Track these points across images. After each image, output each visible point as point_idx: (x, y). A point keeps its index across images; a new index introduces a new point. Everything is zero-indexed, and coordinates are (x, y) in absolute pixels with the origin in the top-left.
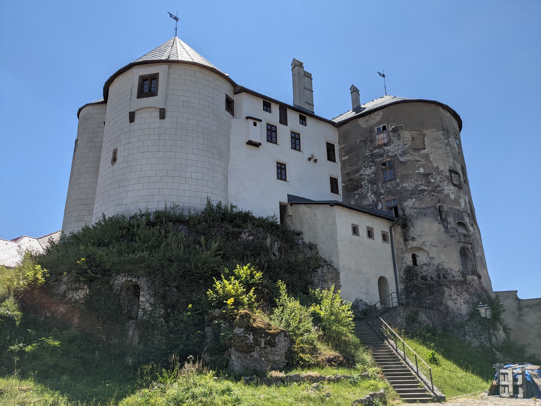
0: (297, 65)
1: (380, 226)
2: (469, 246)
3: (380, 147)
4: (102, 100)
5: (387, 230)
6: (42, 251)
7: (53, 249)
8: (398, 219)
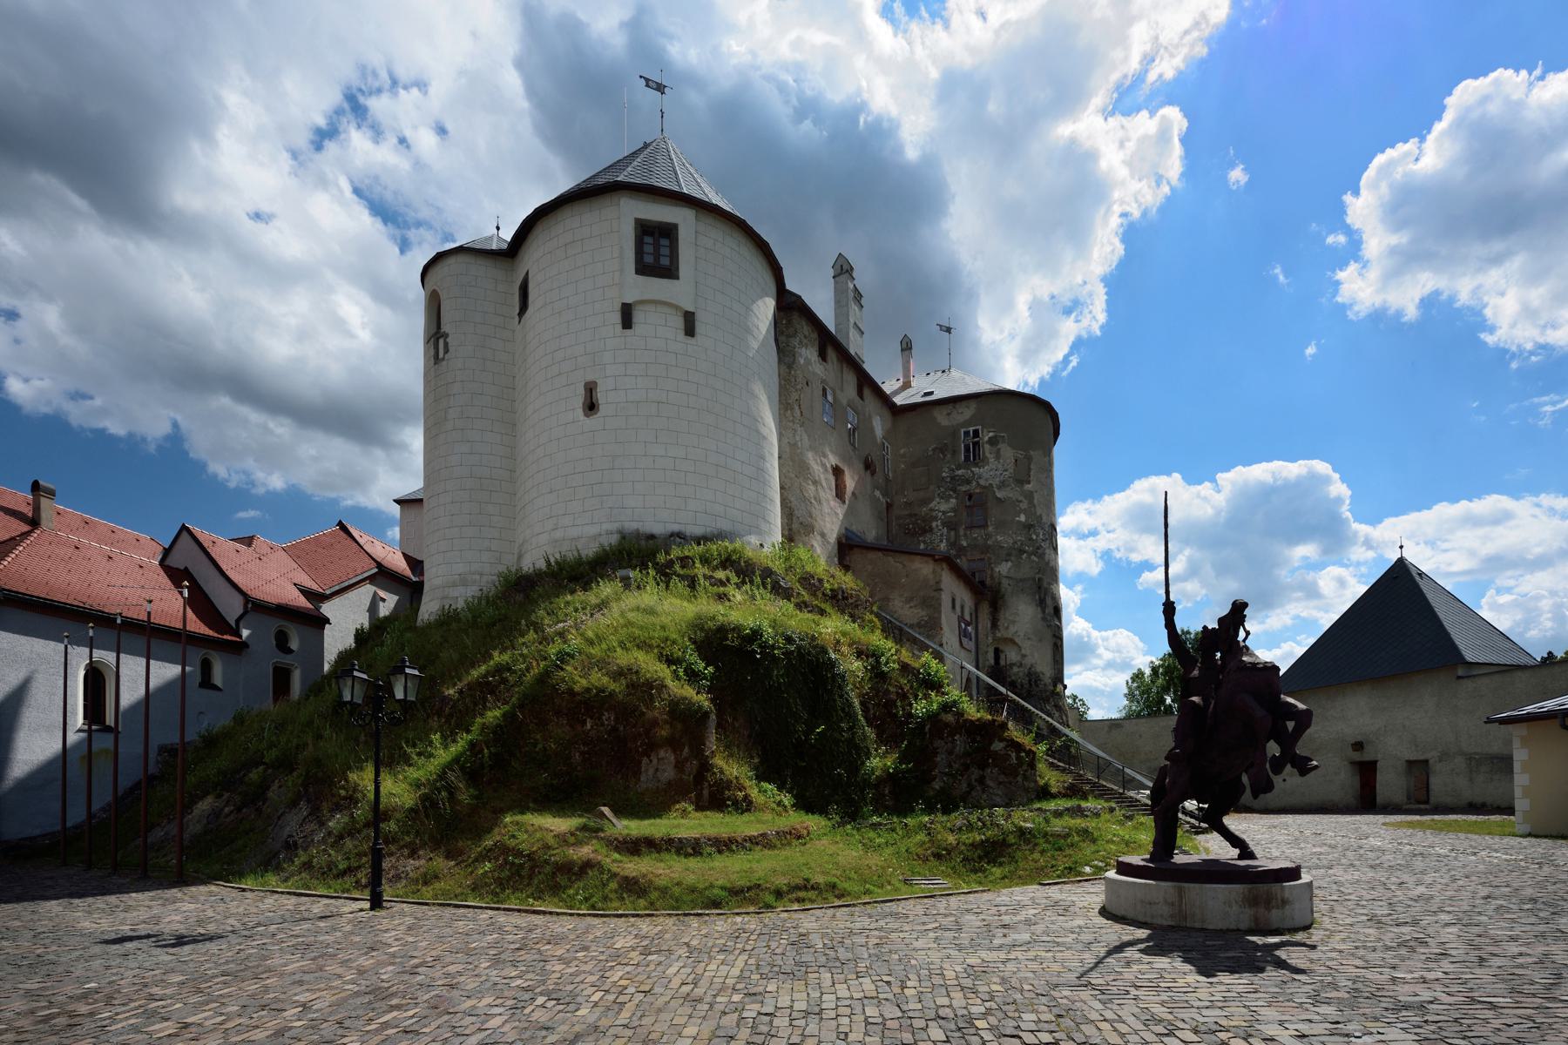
7: (1152, 854)
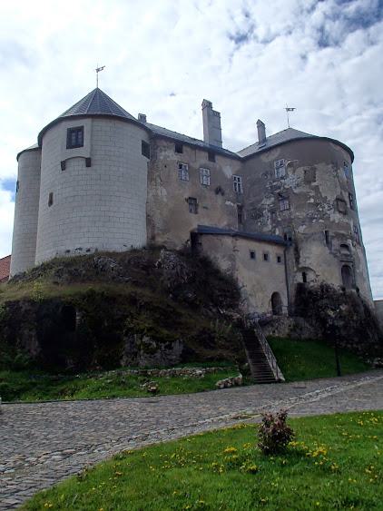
0: (207, 106)
1: (273, 251)
2: (351, 265)
3: (278, 180)
4: (37, 146)
5: (282, 253)
6: (229, 177)
8: (289, 244)
